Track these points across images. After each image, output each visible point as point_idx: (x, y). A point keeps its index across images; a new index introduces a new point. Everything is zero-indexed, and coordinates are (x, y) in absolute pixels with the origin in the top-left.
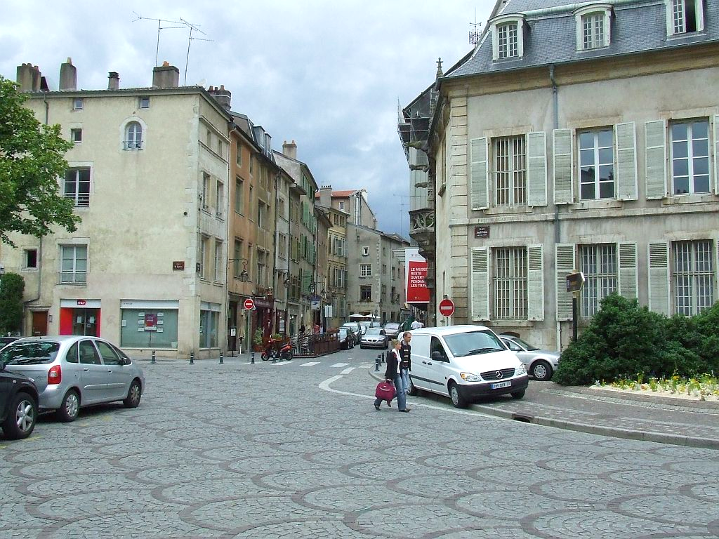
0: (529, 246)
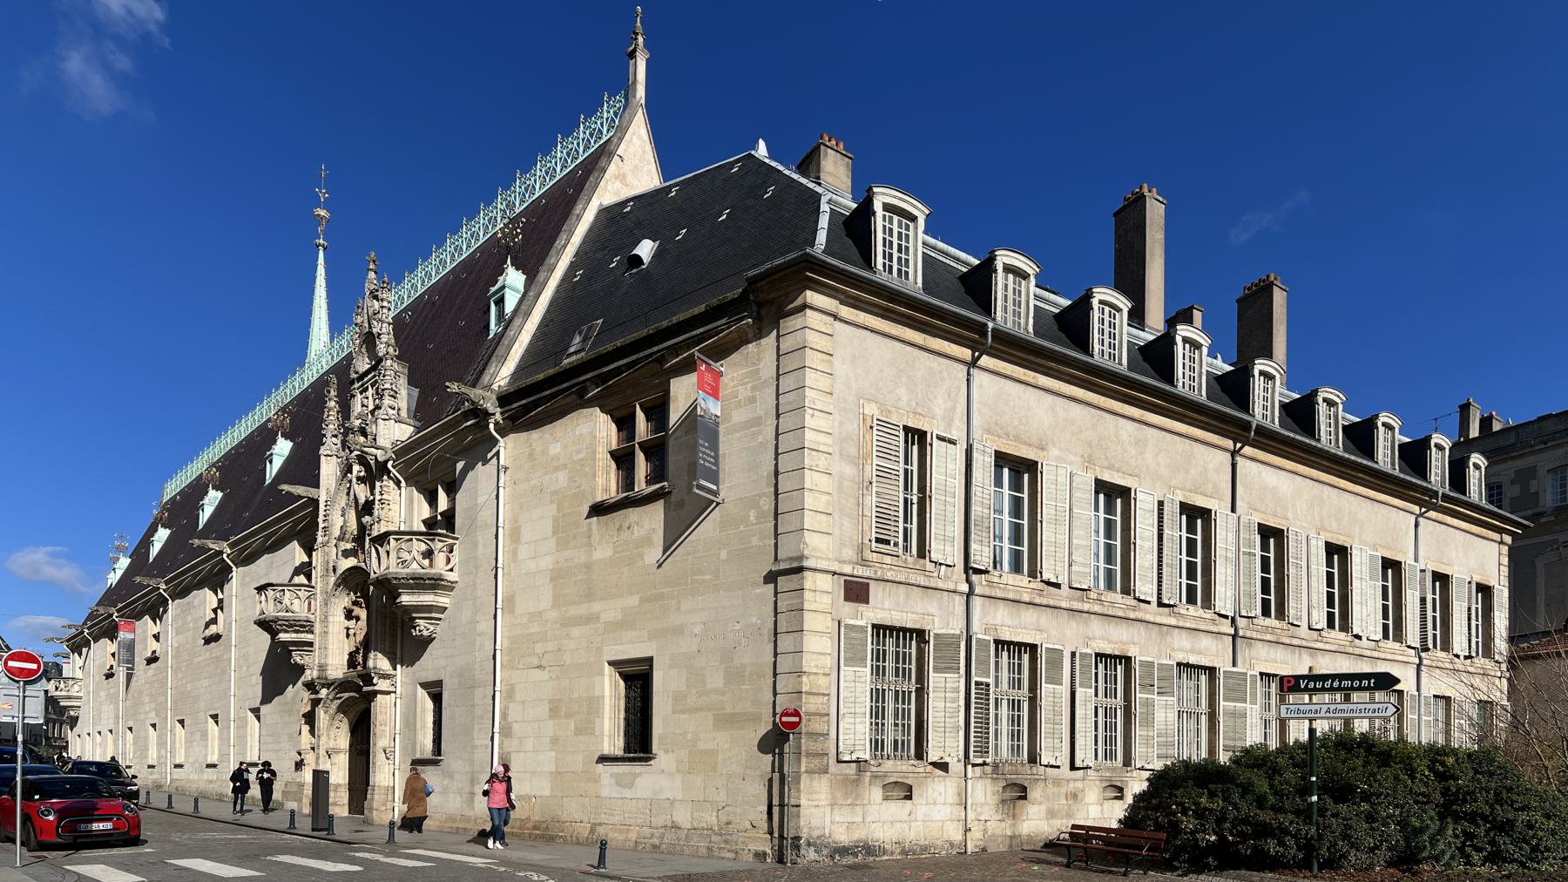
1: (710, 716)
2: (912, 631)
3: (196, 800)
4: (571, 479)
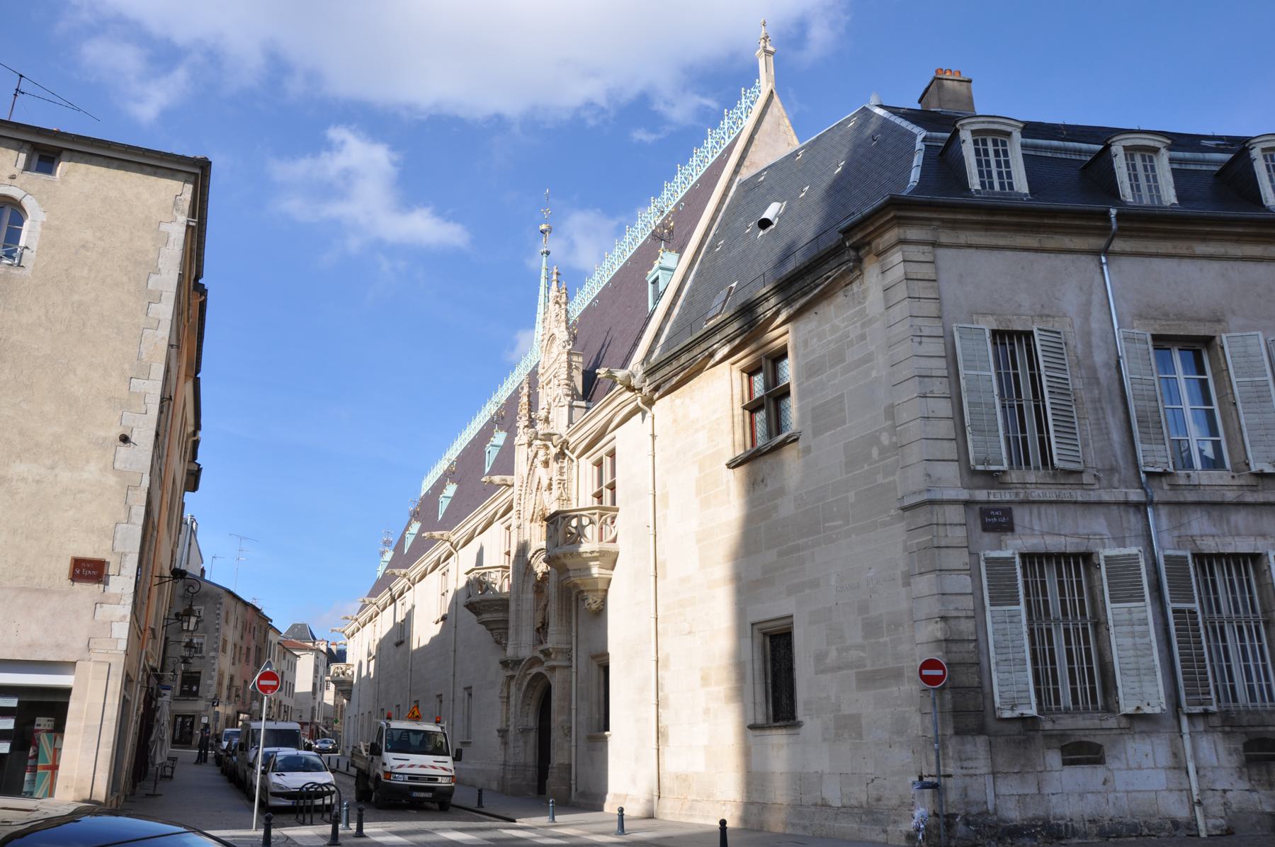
0: (1106, 551)
2: (1076, 556)
3: (480, 791)
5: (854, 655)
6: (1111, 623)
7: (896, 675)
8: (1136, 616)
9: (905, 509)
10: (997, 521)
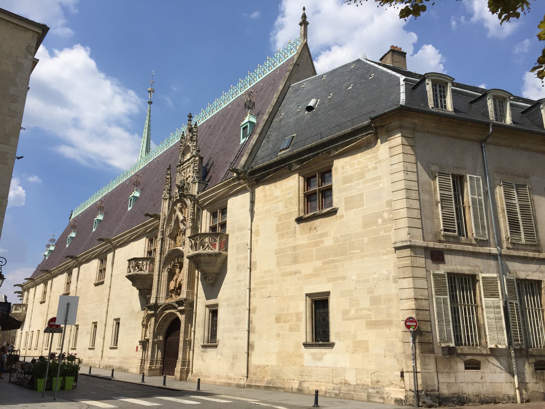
1: (363, 321)
3: (91, 368)
4: (286, 207)
5: (365, 312)
6: (484, 306)
7: (389, 323)
8: (495, 305)
9: (397, 249)
10: (437, 256)
